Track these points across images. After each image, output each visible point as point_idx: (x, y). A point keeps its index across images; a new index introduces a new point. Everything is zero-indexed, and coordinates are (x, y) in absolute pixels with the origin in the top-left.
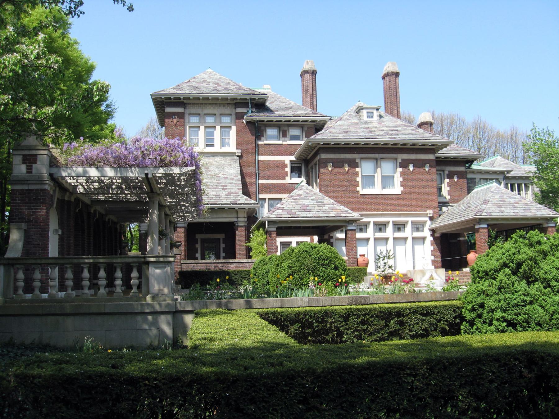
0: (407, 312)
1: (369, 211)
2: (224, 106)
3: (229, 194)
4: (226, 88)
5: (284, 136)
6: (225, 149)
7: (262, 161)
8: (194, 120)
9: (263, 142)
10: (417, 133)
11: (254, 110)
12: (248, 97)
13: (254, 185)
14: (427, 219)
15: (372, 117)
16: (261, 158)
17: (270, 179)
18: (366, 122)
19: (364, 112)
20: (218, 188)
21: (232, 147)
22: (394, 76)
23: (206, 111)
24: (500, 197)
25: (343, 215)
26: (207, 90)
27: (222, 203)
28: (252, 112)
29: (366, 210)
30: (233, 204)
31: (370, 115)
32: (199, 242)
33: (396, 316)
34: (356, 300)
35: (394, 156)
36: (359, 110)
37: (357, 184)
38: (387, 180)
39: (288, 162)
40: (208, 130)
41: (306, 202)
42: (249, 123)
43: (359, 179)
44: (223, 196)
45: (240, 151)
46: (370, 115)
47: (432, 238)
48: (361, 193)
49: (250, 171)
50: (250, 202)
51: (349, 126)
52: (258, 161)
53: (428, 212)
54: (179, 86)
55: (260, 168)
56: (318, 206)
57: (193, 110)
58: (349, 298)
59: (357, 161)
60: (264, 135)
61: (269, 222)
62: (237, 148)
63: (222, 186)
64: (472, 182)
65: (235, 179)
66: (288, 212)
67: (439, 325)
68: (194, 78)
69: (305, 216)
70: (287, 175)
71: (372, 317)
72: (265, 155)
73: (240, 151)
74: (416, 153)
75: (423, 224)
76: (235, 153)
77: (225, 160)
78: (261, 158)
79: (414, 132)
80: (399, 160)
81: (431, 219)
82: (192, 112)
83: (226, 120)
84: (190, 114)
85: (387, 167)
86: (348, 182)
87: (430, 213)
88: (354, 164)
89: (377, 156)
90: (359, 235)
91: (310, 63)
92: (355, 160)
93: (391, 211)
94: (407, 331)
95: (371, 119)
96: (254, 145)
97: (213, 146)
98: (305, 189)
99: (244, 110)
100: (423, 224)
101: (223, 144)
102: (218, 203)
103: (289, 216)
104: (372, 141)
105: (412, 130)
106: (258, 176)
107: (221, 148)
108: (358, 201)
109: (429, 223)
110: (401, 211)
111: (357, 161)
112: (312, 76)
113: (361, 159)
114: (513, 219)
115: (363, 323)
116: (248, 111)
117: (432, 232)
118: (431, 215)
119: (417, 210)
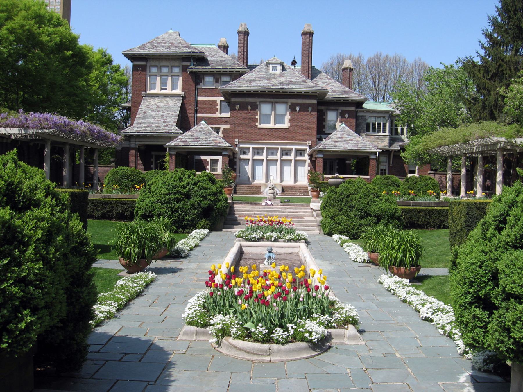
0: (114, 202)
1: (264, 140)
2: (175, 60)
3: (167, 125)
4: (177, 47)
5: (217, 82)
6: (175, 92)
7: (200, 101)
8: (154, 70)
9: (201, 86)
10: (305, 84)
11: (195, 63)
12: (189, 54)
13: (194, 118)
14: (307, 147)
15: (277, 70)
16: (200, 98)
17: (205, 114)
18: (271, 74)
19: (271, 66)
20: (160, 121)
21: (179, 91)
22: (308, 35)
23: (162, 64)
24: (341, 135)
25: (219, 145)
26: (162, 49)
27: (159, 132)
28: (194, 65)
29: (262, 140)
30: (166, 133)
31: (275, 69)
32: (154, 157)
33: (110, 204)
34: (105, 196)
35: (286, 100)
36: (268, 64)
37: (256, 120)
38: (279, 119)
39: (218, 102)
40: (163, 77)
41: (199, 135)
42: (192, 73)
43: (258, 117)
44: (162, 127)
45: (183, 93)
46: (275, 69)
47: (309, 161)
48: (259, 126)
49: (190, 108)
50: (178, 132)
51: (255, 78)
52: (197, 100)
53: (308, 142)
54: (144, 45)
55: (198, 106)
56: (206, 138)
57: (153, 63)
58: (101, 195)
59: (257, 104)
60: (203, 82)
61: (169, 148)
62: (182, 92)
63: (164, 119)
64: (362, 119)
65: (175, 114)
66: (184, 142)
67: (130, 209)
68: (157, 38)
69: (194, 144)
70: (217, 111)
71: (99, 203)
72: (202, 96)
73: (183, 93)
74: (302, 99)
75: (304, 151)
76: (180, 95)
77: (172, 100)
78: (200, 98)
79: (303, 83)
80: (289, 104)
81: (310, 147)
82: (152, 65)
83: (176, 70)
84: (151, 66)
85: (281, 108)
86: (250, 118)
87: (309, 142)
88: (255, 107)
89: (272, 100)
90: (242, 157)
91: (243, 25)
92: (256, 102)
93: (280, 140)
94: (114, 211)
95: (276, 72)
96: (194, 89)
97: (166, 89)
98: (202, 126)
99: (187, 63)
100: (304, 151)
101: (173, 88)
102: (157, 132)
103: (183, 144)
104: (267, 90)
105: (302, 81)
106: (197, 111)
107: (171, 91)
108: (256, 133)
109: (308, 150)
110: (288, 140)
111: (257, 104)
112: (244, 35)
113: (261, 102)
114: (341, 152)
115: (95, 206)
116: (191, 64)
117: (310, 157)
118: (310, 145)
119: (300, 141)
